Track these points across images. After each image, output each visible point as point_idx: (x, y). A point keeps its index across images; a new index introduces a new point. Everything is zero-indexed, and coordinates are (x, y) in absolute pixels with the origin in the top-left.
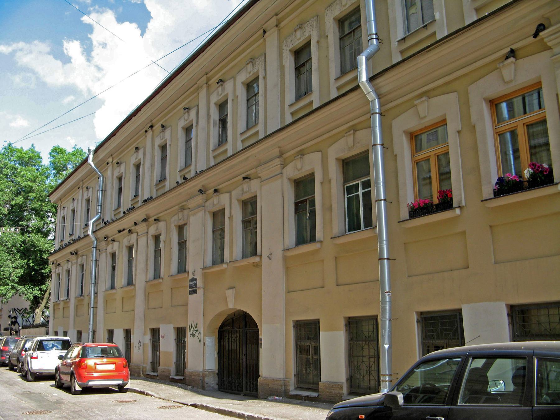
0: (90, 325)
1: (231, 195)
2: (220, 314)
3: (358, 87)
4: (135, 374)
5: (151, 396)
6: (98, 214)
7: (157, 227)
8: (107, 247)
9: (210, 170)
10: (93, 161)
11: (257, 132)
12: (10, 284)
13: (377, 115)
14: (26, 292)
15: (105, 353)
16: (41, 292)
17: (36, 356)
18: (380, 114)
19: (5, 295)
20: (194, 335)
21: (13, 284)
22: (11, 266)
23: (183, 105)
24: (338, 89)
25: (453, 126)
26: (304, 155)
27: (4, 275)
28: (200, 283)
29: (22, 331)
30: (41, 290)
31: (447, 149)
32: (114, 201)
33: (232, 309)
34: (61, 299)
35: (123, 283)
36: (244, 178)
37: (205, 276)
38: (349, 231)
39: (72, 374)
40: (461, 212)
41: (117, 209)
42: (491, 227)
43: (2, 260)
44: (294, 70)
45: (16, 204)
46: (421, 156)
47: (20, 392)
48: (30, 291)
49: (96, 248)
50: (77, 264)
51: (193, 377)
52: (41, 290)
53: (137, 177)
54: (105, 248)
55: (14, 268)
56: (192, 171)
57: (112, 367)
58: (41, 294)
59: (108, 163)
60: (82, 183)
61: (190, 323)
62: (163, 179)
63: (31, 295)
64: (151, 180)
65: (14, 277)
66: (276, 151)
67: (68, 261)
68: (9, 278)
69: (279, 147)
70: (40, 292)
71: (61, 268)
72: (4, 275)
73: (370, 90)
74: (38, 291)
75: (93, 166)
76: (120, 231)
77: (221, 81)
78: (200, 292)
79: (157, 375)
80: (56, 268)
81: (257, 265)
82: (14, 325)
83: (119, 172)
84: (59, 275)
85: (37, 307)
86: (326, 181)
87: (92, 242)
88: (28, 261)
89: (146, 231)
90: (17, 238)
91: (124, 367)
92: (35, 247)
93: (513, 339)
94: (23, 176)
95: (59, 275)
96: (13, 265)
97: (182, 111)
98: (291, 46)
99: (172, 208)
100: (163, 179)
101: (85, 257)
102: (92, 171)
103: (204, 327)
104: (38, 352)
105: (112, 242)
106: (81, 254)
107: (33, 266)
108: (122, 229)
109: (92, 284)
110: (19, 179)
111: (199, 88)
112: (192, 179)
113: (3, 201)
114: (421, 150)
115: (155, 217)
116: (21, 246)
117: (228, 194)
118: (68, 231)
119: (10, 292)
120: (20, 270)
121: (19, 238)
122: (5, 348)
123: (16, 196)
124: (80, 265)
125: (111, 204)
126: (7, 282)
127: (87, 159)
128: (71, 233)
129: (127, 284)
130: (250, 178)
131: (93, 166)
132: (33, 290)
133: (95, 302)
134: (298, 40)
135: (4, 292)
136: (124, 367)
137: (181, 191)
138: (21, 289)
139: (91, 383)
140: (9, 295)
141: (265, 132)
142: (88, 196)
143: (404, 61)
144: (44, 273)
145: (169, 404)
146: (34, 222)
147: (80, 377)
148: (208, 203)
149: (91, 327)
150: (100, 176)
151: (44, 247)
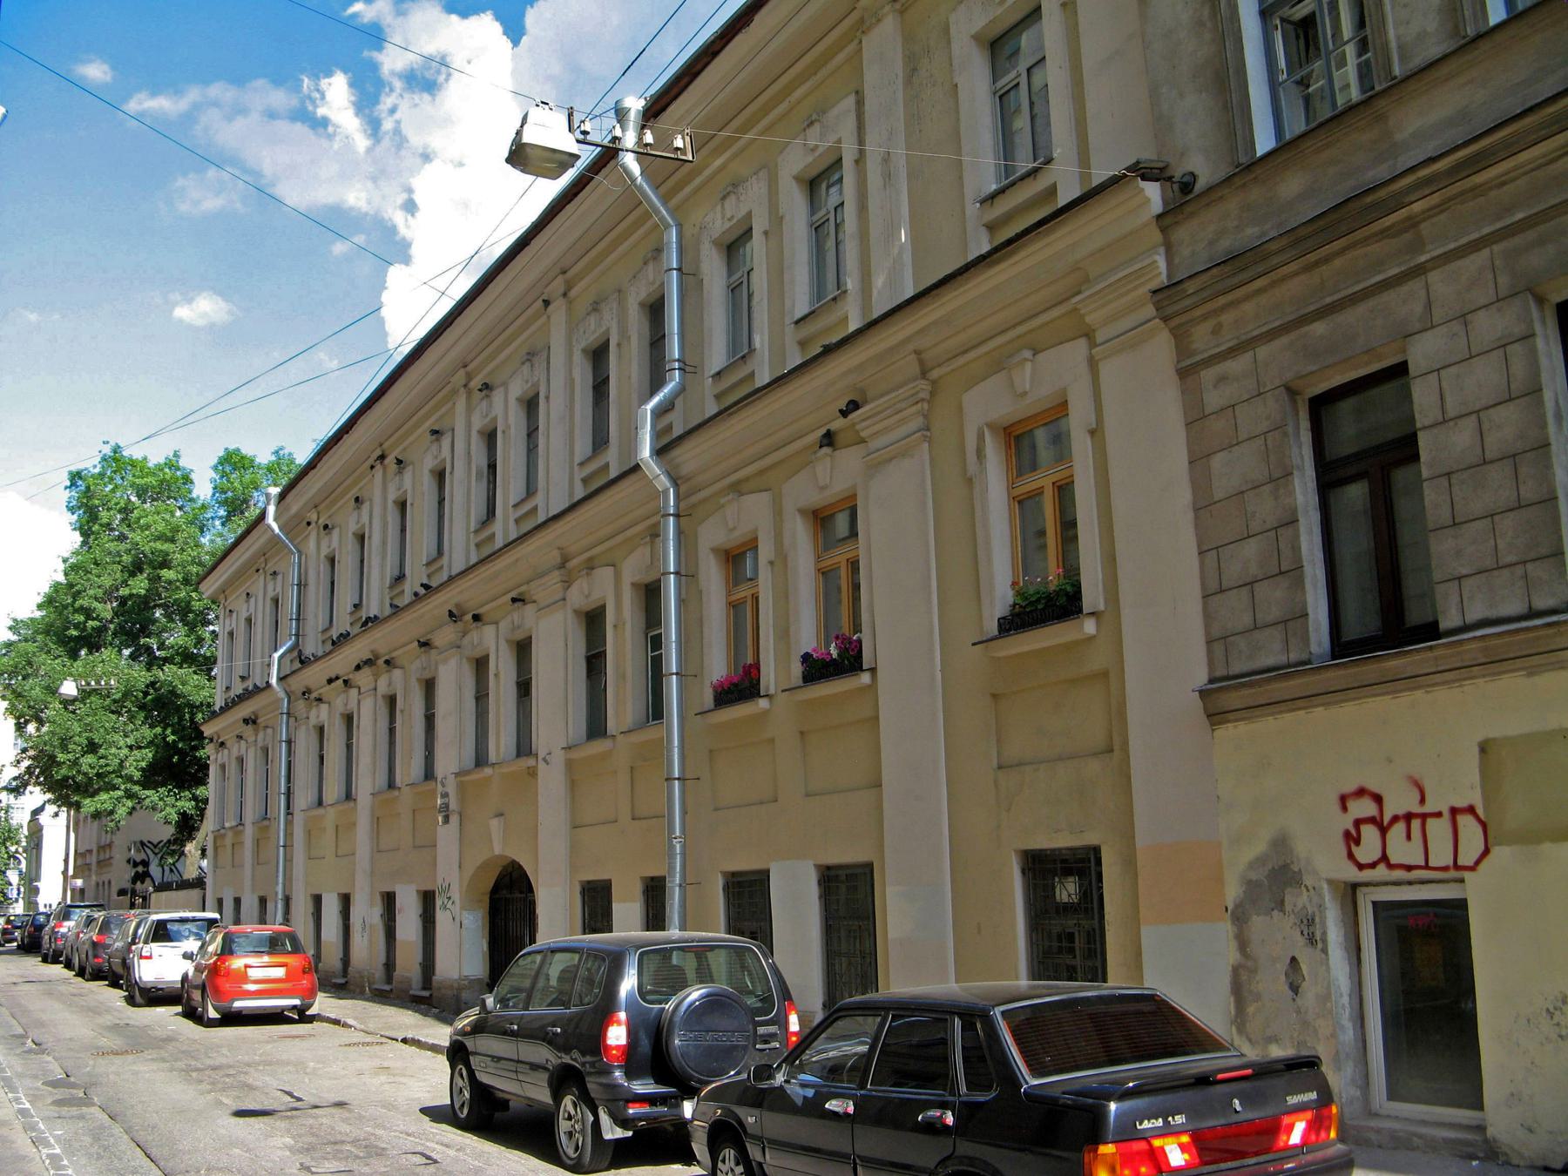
0: (277, 884)
1: (498, 628)
2: (484, 866)
3: (636, 468)
4: (342, 986)
5: (351, 1027)
6: (290, 639)
7: (390, 678)
8: (308, 712)
9: (472, 572)
10: (275, 520)
11: (535, 509)
12: (123, 787)
13: (671, 518)
14: (161, 803)
15: (273, 945)
16: (197, 805)
17: (148, 954)
18: (677, 516)
19: (112, 812)
20: (445, 908)
21: (129, 786)
22: (122, 743)
23: (428, 425)
24: (718, 397)
25: (765, 551)
26: (593, 569)
27: (107, 765)
28: (453, 805)
29: (153, 896)
30: (195, 798)
31: (1068, 474)
32: (320, 609)
33: (501, 857)
34: (227, 825)
35: (336, 796)
36: (514, 600)
37: (461, 788)
38: (653, 720)
39: (203, 988)
40: (771, 702)
41: (434, 560)
42: (802, 733)
43: (102, 730)
44: (591, 390)
45: (131, 595)
46: (1030, 483)
47: (109, 1023)
48: (170, 800)
49: (288, 714)
50: (256, 745)
51: (443, 991)
52: (195, 798)
53: (529, 435)
54: (305, 716)
55: (131, 748)
56: (406, 591)
57: (280, 973)
58: (197, 807)
59: (309, 524)
61: (439, 882)
62: (400, 578)
63: (172, 811)
64: (382, 578)
65: (132, 768)
66: (556, 557)
67: (240, 737)
68: (120, 772)
69: (559, 548)
70: (193, 803)
71: (226, 751)
72: (107, 765)
73: (659, 472)
74: (190, 800)
75: (277, 530)
76: (330, 681)
77: (486, 387)
78: (454, 819)
79: (391, 990)
80: (217, 753)
81: (532, 773)
82: (143, 882)
83: (329, 547)
84: (223, 767)
85: (191, 838)
86: (781, 560)
87: (281, 700)
88: (165, 729)
89: (372, 686)
90: (135, 678)
91: (304, 972)
92: (178, 696)
94: (148, 527)
95: (223, 767)
96: (127, 740)
97: (429, 437)
98: (583, 344)
99: (965, 352)
100: (400, 578)
101: (269, 731)
102: (631, 199)
103: (460, 892)
104: (153, 945)
105: (315, 703)
106: (263, 725)
107: (174, 740)
108: (334, 676)
109: (279, 794)
110: (136, 536)
111: (455, 392)
112: (443, 585)
113: (99, 587)
114: (1034, 467)
115: (387, 658)
116: (146, 694)
117: (494, 626)
118: (345, 598)
119: (124, 805)
120: (144, 751)
121: (140, 676)
122: (101, 937)
123: (133, 574)
124: (261, 748)
125: (316, 616)
126: (115, 781)
127: (262, 516)
128: (246, 675)
129: (515, 753)
130: (523, 601)
131: (277, 530)
132: (177, 800)
133: (289, 834)
134: (729, 220)
135: (109, 806)
136: (304, 972)
137: (422, 611)
138: (147, 797)
139: (238, 1004)
140: (121, 811)
141: (1085, 177)
142: (329, 547)
143: (996, 250)
144: (201, 758)
145: (369, 1039)
146: (177, 637)
147: (217, 991)
148: (466, 641)
149: (280, 889)
150: (667, 226)
151: (197, 698)
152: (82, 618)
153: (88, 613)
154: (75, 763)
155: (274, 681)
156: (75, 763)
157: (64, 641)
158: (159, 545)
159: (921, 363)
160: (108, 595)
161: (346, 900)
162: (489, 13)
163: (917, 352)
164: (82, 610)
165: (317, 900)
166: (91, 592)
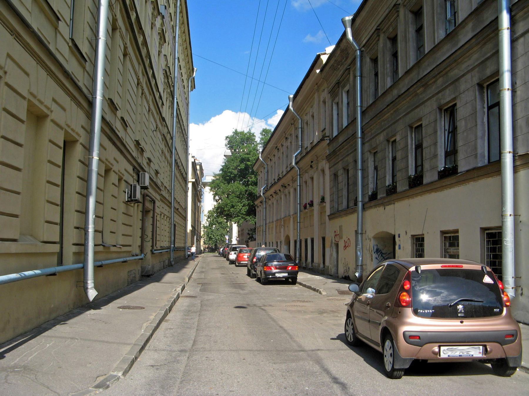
10: (261, 157)
60: (284, 134)
66: (291, 178)
93: (446, 251)
121: (243, 188)
123: (241, 163)
139: (242, 262)
152: (230, 174)
153: (231, 173)
154: (229, 210)
155: (262, 194)
156: (229, 210)
157: (225, 180)
158: (246, 156)
159: (317, 157)
160: (236, 168)
161: (273, 243)
162: (97, 293)
163: (316, 155)
164: (229, 172)
165: (270, 243)
166: (231, 168)
